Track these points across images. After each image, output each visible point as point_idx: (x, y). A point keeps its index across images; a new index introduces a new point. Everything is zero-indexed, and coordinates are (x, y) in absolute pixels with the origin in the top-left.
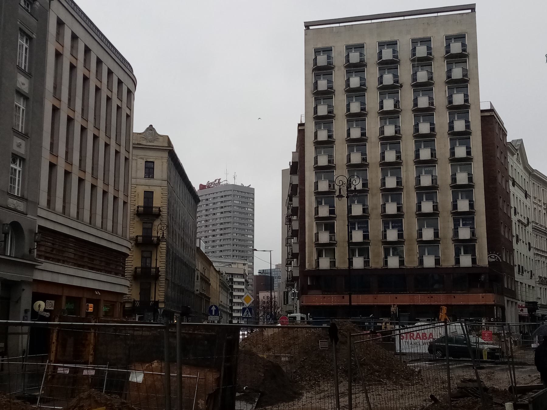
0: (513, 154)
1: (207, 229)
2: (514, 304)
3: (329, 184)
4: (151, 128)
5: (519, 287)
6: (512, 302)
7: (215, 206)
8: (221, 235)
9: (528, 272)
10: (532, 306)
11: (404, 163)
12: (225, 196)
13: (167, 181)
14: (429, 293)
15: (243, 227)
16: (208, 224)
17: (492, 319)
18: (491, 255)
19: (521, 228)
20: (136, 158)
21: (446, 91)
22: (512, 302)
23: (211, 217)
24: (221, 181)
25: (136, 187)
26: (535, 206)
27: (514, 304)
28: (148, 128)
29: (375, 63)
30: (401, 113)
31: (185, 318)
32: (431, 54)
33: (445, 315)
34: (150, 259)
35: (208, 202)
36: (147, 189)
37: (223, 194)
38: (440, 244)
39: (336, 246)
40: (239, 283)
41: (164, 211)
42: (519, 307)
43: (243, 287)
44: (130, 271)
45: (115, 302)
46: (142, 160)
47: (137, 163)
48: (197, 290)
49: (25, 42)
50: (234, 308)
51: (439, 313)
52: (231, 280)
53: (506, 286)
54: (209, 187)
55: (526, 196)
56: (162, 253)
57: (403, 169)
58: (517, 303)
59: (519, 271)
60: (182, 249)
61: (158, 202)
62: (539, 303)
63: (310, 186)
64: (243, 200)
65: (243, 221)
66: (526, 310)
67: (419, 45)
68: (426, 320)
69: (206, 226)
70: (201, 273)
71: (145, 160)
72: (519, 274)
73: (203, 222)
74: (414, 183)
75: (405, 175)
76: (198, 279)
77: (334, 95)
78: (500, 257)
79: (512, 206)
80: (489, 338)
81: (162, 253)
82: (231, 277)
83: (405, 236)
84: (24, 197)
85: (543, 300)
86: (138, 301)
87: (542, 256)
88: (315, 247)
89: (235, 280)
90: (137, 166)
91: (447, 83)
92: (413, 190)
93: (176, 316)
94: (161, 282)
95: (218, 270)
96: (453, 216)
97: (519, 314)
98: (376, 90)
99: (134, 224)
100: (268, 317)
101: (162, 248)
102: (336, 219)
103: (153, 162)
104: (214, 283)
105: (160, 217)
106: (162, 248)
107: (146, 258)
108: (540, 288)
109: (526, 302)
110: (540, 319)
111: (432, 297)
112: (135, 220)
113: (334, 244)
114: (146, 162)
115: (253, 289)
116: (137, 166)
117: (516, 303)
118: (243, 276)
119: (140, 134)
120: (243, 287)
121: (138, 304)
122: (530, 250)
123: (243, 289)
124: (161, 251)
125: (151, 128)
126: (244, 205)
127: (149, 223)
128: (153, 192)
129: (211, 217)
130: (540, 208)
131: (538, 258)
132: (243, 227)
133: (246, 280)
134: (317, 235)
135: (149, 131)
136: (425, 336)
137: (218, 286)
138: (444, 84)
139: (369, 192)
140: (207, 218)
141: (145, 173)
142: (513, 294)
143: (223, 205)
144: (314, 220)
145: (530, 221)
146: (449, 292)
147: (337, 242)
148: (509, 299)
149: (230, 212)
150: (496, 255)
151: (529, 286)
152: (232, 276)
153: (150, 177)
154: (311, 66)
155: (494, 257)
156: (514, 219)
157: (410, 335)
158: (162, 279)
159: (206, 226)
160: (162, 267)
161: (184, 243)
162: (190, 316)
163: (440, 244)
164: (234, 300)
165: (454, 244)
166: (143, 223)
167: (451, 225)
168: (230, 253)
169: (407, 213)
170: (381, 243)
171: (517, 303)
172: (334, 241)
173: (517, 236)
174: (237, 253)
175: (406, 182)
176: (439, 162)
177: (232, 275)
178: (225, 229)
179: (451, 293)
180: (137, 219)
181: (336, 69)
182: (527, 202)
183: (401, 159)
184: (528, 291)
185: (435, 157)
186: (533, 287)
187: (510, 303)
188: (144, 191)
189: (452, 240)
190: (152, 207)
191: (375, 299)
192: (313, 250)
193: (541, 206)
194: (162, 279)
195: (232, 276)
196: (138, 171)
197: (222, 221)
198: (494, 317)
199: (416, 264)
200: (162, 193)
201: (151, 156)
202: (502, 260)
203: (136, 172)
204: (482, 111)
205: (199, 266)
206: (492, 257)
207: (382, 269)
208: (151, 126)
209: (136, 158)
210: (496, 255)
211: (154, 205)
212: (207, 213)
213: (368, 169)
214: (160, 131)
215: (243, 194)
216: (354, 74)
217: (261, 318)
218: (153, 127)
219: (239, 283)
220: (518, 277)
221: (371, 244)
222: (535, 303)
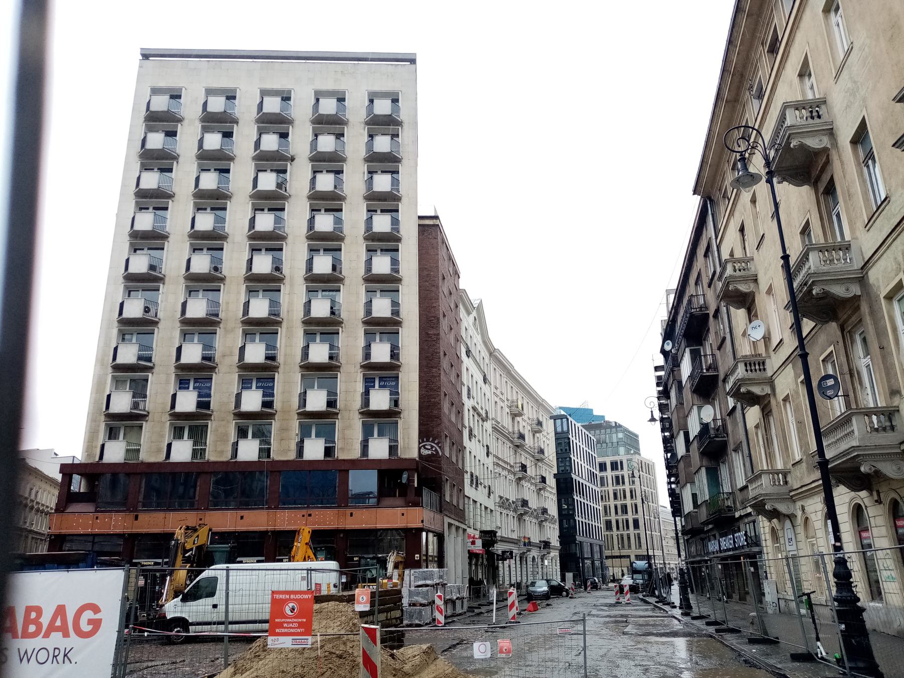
0: (469, 313)
2: (461, 531)
5: (471, 507)
6: (457, 528)
9: (485, 487)
10: (489, 538)
11: (287, 281)
14: (304, 508)
17: (416, 555)
18: (426, 445)
19: (476, 421)
21: (364, 173)
22: (457, 528)
26: (497, 400)
27: (461, 531)
29: (252, 121)
30: (289, 200)
32: (397, 271)
33: (305, 547)
38: (338, 419)
39: (147, 421)
42: (469, 536)
51: (293, 543)
53: (448, 499)
55: (485, 380)
58: (466, 530)
59: (472, 481)
62: (498, 534)
66: (479, 543)
72: (471, 486)
74: (302, 314)
75: (287, 300)
77: (177, 162)
78: (440, 447)
79: (465, 382)
80: (301, 625)
83: (277, 405)
84: (766, 633)
85: (503, 531)
87: (504, 468)
97: (470, 549)
98: (250, 160)
102: (154, 370)
108: (501, 513)
109: (481, 532)
110: (500, 557)
111: (310, 515)
117: (464, 530)
122: (488, 456)
130: (502, 404)
131: (498, 470)
138: (363, 162)
139: (221, 325)
142: (460, 515)
145: (490, 416)
146: (343, 505)
147: (149, 413)
148: (452, 522)
150: (433, 444)
151: (486, 508)
154: (143, 113)
155: (429, 447)
156: (468, 403)
162: (136, 564)
163: (338, 419)
165: (361, 420)
167: (360, 387)
169: (285, 364)
170: (233, 415)
171: (466, 530)
173: (471, 431)
175: (288, 312)
176: (347, 281)
179: (346, 506)
181: (185, 123)
182: (486, 388)
183: (281, 273)
184: (483, 522)
185: (341, 273)
186: (491, 511)
187: (453, 529)
189: (360, 413)
192: (99, 426)
193: (503, 401)
198: (420, 553)
199: (292, 456)
202: (443, 453)
204: (420, 218)
206: (426, 447)
207: (227, 463)
210: (433, 444)
216: (320, 293)
220: (469, 490)
222: (492, 533)
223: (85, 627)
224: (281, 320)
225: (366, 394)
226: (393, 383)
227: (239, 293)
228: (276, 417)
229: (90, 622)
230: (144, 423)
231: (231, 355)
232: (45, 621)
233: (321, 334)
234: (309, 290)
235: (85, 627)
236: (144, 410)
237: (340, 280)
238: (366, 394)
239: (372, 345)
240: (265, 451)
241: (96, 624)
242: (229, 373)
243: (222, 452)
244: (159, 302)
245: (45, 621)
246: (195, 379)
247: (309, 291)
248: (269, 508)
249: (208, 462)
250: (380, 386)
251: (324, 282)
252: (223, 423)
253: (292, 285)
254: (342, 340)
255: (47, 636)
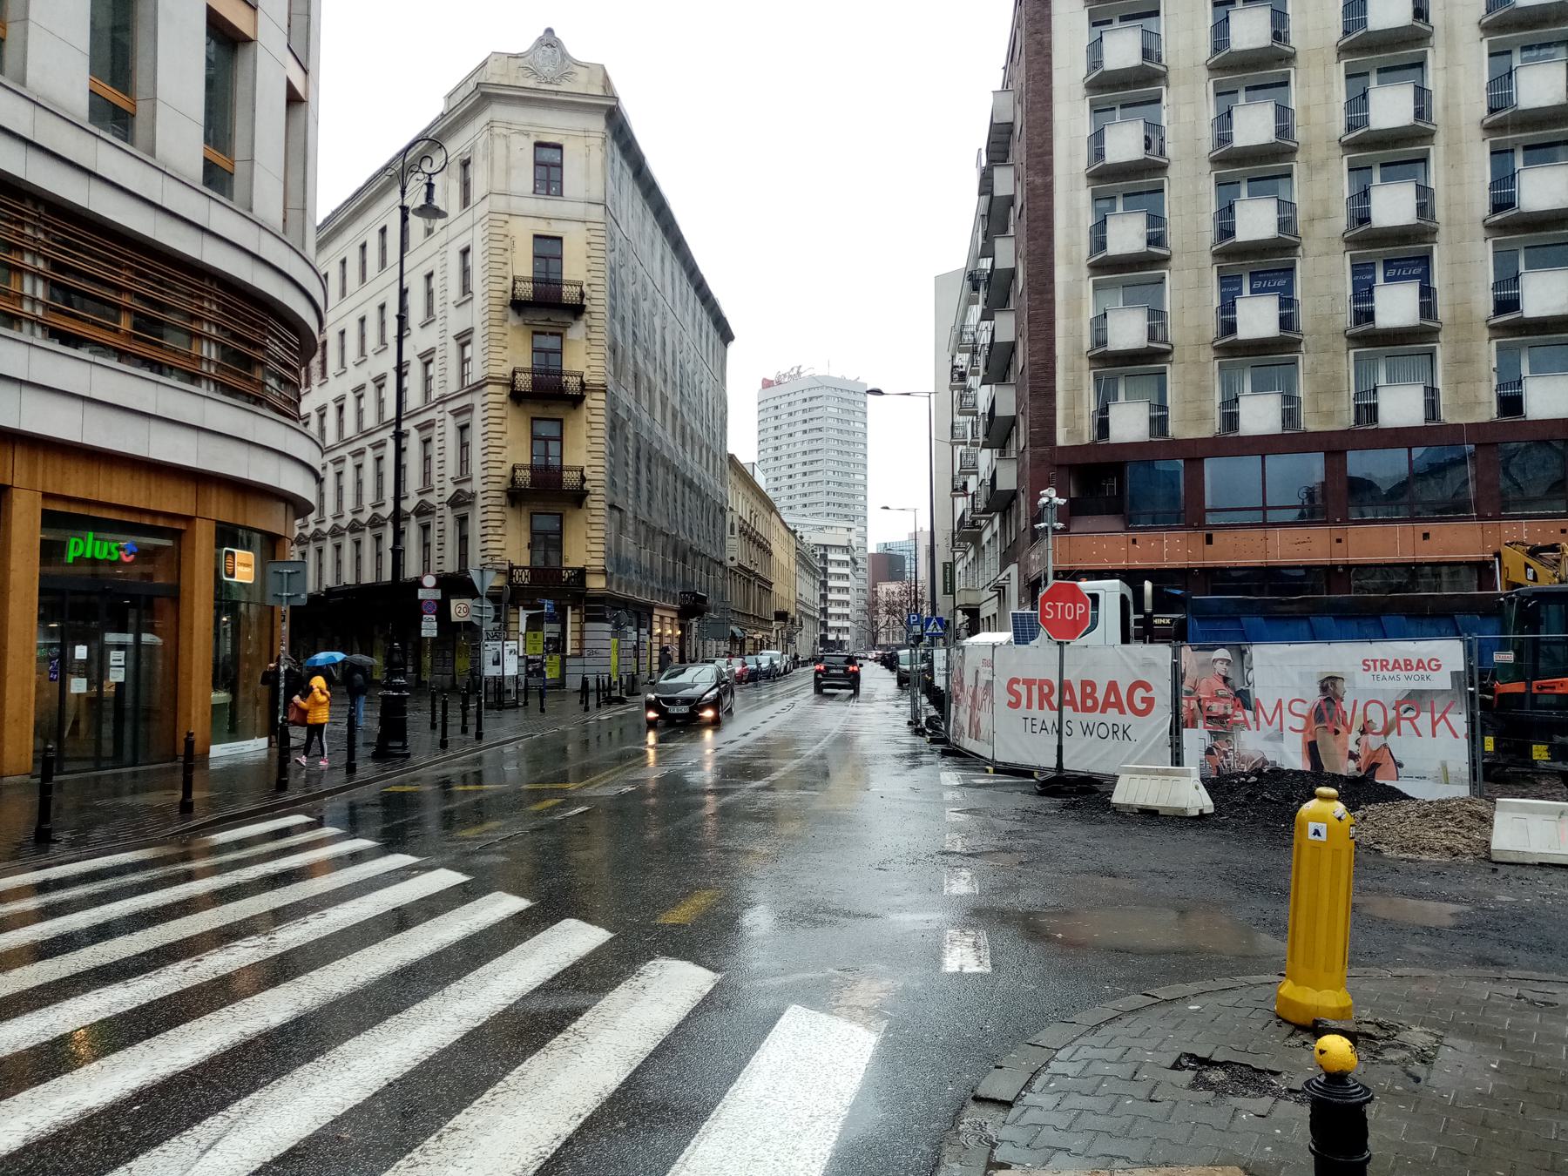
1: (777, 463)
3: (1147, 138)
4: (549, 40)
7: (792, 419)
8: (805, 474)
12: (811, 399)
13: (603, 207)
15: (845, 458)
16: (778, 453)
20: (505, 132)
23: (785, 439)
24: (801, 370)
25: (506, 222)
28: (540, 39)
31: (695, 625)
34: (558, 443)
35: (778, 412)
36: (543, 229)
37: (807, 395)
40: (839, 563)
41: (598, 302)
43: (846, 571)
44: (499, 479)
45: (189, 519)
46: (523, 139)
47: (508, 147)
48: (732, 559)
49: (658, 390)
50: (830, 611)
52: (824, 557)
54: (779, 383)
56: (594, 426)
57: (1435, 59)
60: (679, 440)
61: (575, 268)
63: (1070, 155)
64: (846, 406)
65: (845, 448)
67: (1120, 208)
68: (1168, 621)
69: (776, 458)
70: (741, 518)
71: (533, 139)
73: (770, 451)
76: (732, 533)
81: (594, 426)
82: (822, 552)
86: (524, 568)
88: (1091, 369)
89: (830, 557)
90: (508, 157)
91: (1344, 50)
92: (1477, 133)
93: (662, 617)
94: (594, 512)
95: (792, 528)
96: (1496, 338)
99: (505, 334)
100: (1081, 608)
101: (595, 411)
102: (1172, 264)
103: (559, 147)
104: (782, 553)
105: (586, 316)
106: (595, 411)
107: (546, 440)
112: (507, 325)
113: (1163, 355)
114: (539, 145)
115: (866, 576)
116: (508, 157)
118: (846, 549)
119: (517, 57)
120: (846, 571)
121: (523, 578)
123: (847, 576)
124: (590, 420)
125: (549, 40)
126: (846, 416)
127: (552, 334)
128: (560, 239)
129: (785, 439)
132: (845, 458)
133: (853, 559)
134: (1100, 321)
135: (544, 48)
136: (1092, 696)
137: (792, 560)
140: (777, 443)
141: (535, 179)
143: (807, 416)
144: (1085, 272)
149: (820, 429)
152: (826, 550)
153: (551, 192)
157: (1041, 689)
158: (595, 505)
159: (776, 458)
160: (593, 469)
161: (683, 428)
164: (830, 597)
166: (535, 333)
168: (825, 509)
169: (1448, 225)
170: (1345, 340)
172: (1161, 342)
174: (835, 510)
175: (1446, 108)
177: (825, 547)
178: (812, 462)
180: (514, 320)
188: (536, 237)
189: (1215, 348)
190: (560, 283)
191: (1339, 541)
192: (1081, 378)
194: (595, 505)
195: (826, 550)
196: (513, 171)
197: (806, 447)
200: (588, 243)
201: (553, 125)
203: (508, 172)
205: (739, 505)
208: (549, 31)
209: (505, 132)
211: (567, 275)
212: (778, 433)
213: (1164, 88)
214: (577, 49)
215: (845, 395)
216: (1118, 112)
217: (883, 630)
218: (557, 35)
219: (839, 563)
221: (1303, 349)
223: (1141, 706)
224: (1166, 161)
225: (1228, 307)
226: (1281, 283)
227: (1328, 83)
228: (1441, 337)
229: (1144, 700)
230: (1168, 366)
231: (1326, 216)
232: (1100, 695)
233: (1526, 148)
234: (1096, 109)
235: (1141, 706)
236: (1165, 342)
237: (1288, 58)
238: (1228, 307)
239: (1110, 221)
240: (1159, 423)
241: (1150, 702)
242: (1327, 254)
243: (1330, 415)
244: (1164, 123)
245: (1100, 695)
246: (1251, 273)
247: (1096, 111)
248: (1481, 517)
249: (1305, 433)
250: (1253, 291)
251: (1531, 28)
252: (1327, 357)
253: (1450, 46)
254: (1300, 191)
255: (1103, 711)
